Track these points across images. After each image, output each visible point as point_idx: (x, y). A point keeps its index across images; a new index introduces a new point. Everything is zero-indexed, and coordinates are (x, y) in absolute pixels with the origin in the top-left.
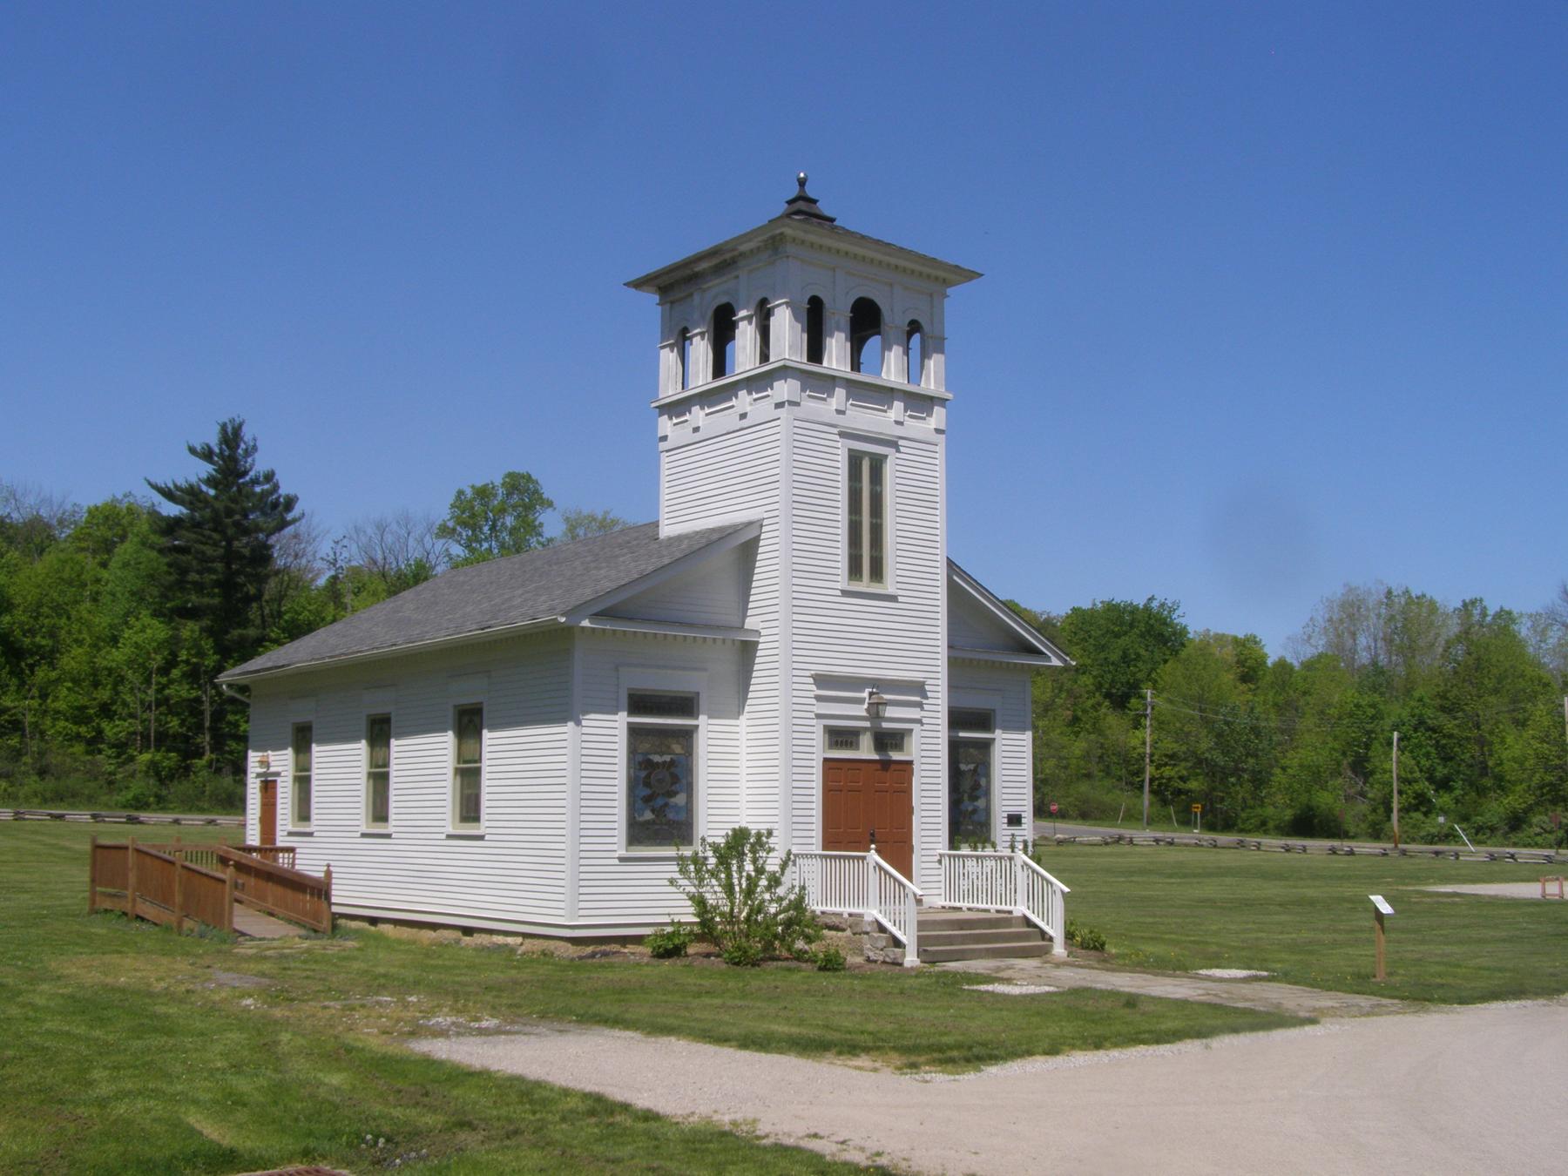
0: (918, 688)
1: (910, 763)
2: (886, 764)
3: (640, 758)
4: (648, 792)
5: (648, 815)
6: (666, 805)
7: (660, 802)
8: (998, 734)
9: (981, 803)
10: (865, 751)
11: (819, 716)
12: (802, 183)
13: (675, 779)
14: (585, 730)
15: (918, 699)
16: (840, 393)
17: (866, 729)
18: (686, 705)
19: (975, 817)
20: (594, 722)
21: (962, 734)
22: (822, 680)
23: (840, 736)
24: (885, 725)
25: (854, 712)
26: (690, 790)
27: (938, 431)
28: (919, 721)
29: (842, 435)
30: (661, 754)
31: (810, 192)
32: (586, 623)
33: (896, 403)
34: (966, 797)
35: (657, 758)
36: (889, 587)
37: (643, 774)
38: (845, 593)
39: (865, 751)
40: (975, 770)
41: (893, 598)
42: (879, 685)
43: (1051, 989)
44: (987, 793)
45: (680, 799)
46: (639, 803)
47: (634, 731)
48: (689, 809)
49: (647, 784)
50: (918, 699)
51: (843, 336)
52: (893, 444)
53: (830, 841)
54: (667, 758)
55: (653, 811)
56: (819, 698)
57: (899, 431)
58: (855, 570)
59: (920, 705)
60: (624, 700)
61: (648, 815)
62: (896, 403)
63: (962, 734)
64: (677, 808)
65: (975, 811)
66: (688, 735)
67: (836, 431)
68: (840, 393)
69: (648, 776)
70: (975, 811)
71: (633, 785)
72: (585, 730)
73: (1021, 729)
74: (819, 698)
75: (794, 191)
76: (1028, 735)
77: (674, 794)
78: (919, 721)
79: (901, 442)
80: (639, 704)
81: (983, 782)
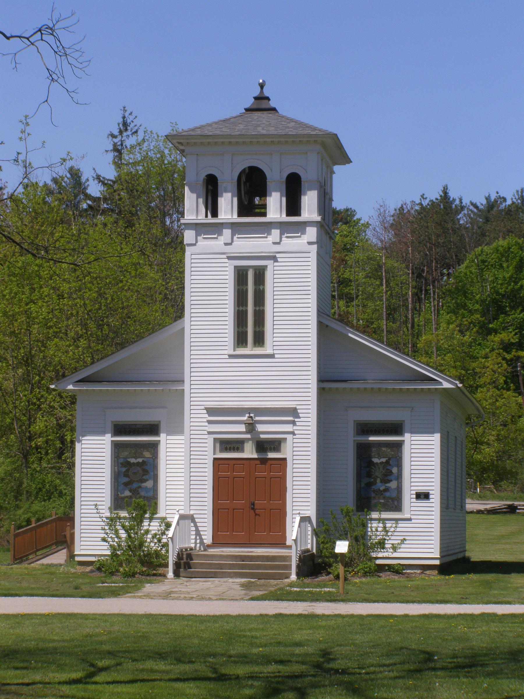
0: (294, 412)
1: (285, 459)
2: (264, 461)
3: (121, 461)
4: (126, 480)
5: (127, 493)
6: (140, 487)
7: (135, 485)
8: (408, 439)
9: (393, 485)
10: (249, 452)
11: (210, 433)
12: (262, 86)
13: (146, 472)
14: (83, 446)
15: (291, 418)
16: (227, 232)
17: (248, 439)
18: (153, 429)
19: (387, 494)
20: (436, 435)
21: (372, 438)
22: (211, 411)
23: (227, 445)
24: (262, 436)
25: (236, 429)
26: (156, 478)
27: (310, 243)
28: (293, 433)
29: (229, 258)
30: (136, 458)
31: (267, 92)
32: (70, 387)
33: (273, 231)
34: (378, 481)
35: (133, 460)
36: (268, 350)
37: (124, 470)
38: (231, 356)
39: (249, 452)
40: (387, 462)
41: (272, 356)
42: (249, 410)
43: (266, 592)
44: (399, 477)
45: (149, 484)
46: (121, 487)
47: (117, 447)
48: (155, 489)
49: (126, 475)
50: (291, 418)
51: (229, 195)
52: (274, 259)
53: (358, 510)
54: (140, 460)
55: (130, 491)
56: (210, 422)
57: (277, 248)
58: (241, 339)
59: (294, 423)
60: (110, 426)
61: (127, 493)
62: (273, 231)
63: (372, 438)
64: (147, 489)
65: (387, 490)
66: (155, 446)
67: (225, 256)
68: (227, 232)
69: (127, 471)
70: (387, 490)
71: (116, 477)
72: (83, 446)
73: (430, 431)
74: (210, 422)
75: (257, 92)
76: (437, 438)
77: (145, 481)
78: (293, 433)
79: (278, 255)
80: (120, 429)
81: (395, 470)
